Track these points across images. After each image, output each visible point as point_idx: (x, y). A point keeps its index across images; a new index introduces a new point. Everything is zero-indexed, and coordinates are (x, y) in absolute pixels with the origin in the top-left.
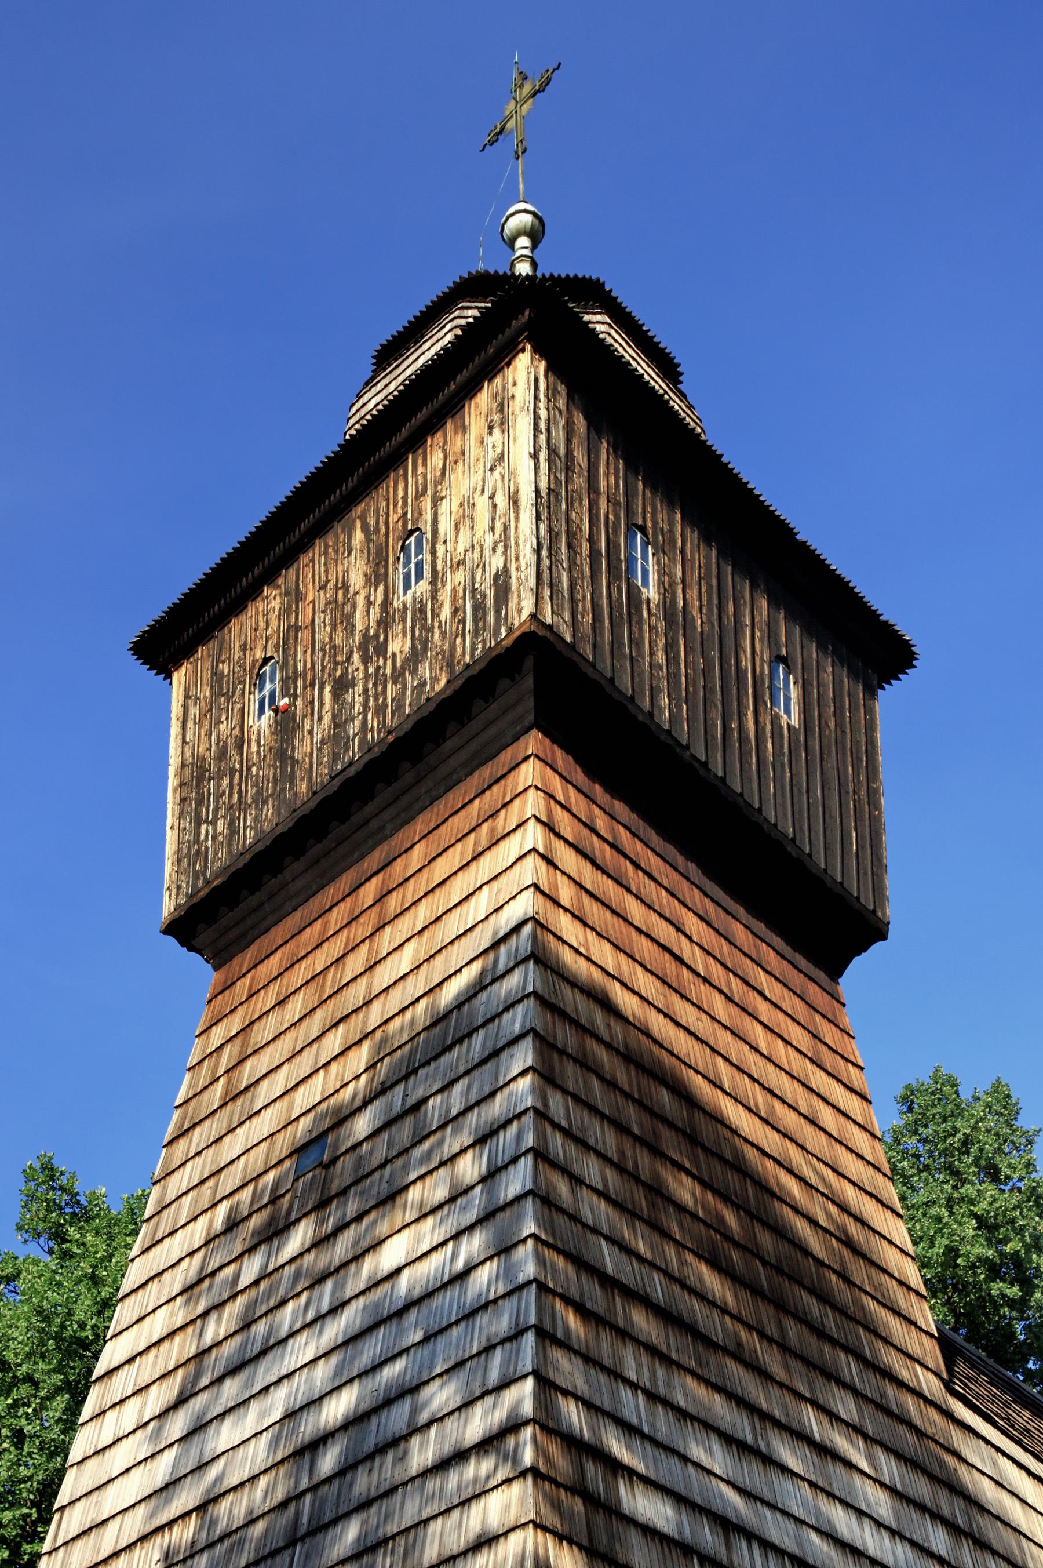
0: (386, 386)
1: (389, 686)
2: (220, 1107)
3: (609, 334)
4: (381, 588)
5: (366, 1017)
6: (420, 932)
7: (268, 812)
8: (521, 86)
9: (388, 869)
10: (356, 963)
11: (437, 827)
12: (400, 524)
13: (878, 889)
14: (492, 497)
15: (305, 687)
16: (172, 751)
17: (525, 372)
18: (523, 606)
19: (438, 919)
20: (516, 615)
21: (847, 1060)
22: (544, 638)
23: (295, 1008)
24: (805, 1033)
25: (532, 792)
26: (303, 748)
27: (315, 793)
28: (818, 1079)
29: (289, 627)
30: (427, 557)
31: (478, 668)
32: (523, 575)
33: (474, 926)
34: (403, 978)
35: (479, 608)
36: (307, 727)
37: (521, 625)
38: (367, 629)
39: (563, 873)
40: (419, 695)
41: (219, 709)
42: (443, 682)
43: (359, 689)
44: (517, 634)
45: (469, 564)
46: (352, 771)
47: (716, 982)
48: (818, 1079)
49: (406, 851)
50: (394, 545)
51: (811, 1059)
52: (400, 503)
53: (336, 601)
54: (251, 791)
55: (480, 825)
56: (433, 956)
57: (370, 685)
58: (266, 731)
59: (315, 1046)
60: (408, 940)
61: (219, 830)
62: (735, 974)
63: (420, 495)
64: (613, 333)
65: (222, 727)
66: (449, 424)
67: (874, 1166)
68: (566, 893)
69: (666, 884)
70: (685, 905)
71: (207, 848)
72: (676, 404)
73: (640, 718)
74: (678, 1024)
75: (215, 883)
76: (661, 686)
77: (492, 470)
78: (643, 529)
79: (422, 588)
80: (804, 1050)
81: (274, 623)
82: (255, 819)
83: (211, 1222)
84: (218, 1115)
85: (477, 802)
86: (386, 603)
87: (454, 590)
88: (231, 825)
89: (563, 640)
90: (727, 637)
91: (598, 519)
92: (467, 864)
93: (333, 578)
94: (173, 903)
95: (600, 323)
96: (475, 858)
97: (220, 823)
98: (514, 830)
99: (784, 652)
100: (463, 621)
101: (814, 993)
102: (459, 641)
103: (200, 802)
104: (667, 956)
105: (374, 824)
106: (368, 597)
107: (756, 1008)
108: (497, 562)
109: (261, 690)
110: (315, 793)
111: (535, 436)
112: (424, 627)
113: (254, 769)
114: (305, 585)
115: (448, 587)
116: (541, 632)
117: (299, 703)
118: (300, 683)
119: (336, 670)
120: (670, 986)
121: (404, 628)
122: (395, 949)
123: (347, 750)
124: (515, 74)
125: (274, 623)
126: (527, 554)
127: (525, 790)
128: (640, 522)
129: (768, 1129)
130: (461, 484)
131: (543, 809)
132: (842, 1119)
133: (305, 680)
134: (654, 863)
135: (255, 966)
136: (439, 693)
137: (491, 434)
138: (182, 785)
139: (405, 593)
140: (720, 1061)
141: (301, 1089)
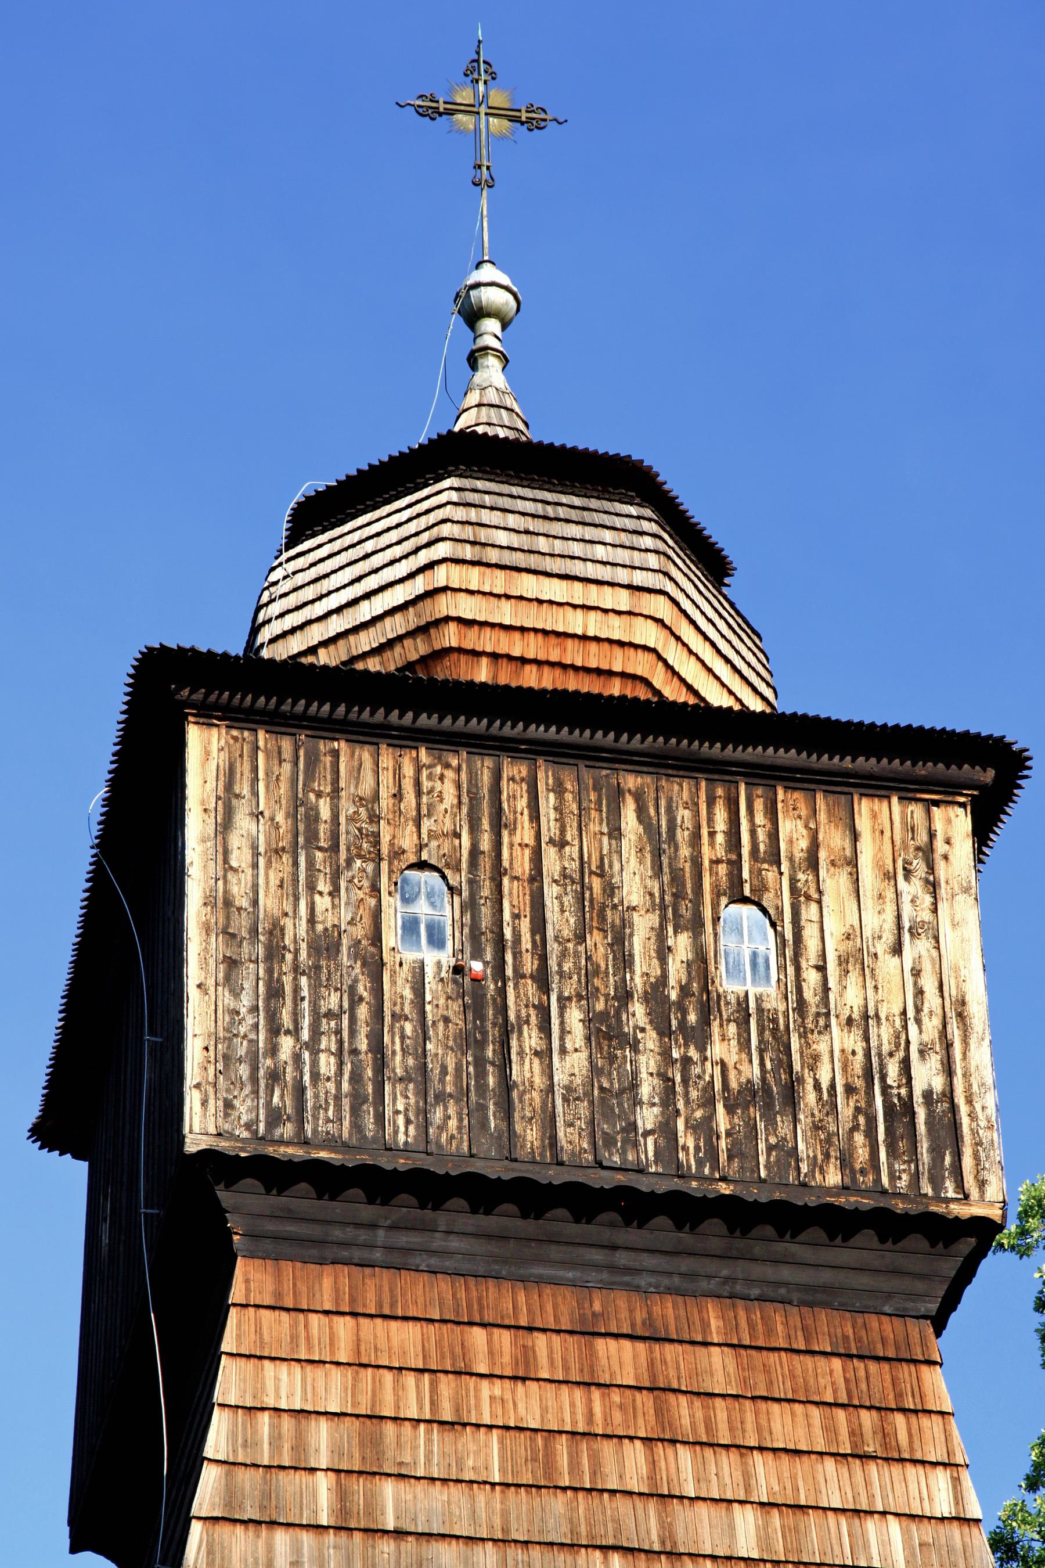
75: (323, 1155)
105: (622, 1258)
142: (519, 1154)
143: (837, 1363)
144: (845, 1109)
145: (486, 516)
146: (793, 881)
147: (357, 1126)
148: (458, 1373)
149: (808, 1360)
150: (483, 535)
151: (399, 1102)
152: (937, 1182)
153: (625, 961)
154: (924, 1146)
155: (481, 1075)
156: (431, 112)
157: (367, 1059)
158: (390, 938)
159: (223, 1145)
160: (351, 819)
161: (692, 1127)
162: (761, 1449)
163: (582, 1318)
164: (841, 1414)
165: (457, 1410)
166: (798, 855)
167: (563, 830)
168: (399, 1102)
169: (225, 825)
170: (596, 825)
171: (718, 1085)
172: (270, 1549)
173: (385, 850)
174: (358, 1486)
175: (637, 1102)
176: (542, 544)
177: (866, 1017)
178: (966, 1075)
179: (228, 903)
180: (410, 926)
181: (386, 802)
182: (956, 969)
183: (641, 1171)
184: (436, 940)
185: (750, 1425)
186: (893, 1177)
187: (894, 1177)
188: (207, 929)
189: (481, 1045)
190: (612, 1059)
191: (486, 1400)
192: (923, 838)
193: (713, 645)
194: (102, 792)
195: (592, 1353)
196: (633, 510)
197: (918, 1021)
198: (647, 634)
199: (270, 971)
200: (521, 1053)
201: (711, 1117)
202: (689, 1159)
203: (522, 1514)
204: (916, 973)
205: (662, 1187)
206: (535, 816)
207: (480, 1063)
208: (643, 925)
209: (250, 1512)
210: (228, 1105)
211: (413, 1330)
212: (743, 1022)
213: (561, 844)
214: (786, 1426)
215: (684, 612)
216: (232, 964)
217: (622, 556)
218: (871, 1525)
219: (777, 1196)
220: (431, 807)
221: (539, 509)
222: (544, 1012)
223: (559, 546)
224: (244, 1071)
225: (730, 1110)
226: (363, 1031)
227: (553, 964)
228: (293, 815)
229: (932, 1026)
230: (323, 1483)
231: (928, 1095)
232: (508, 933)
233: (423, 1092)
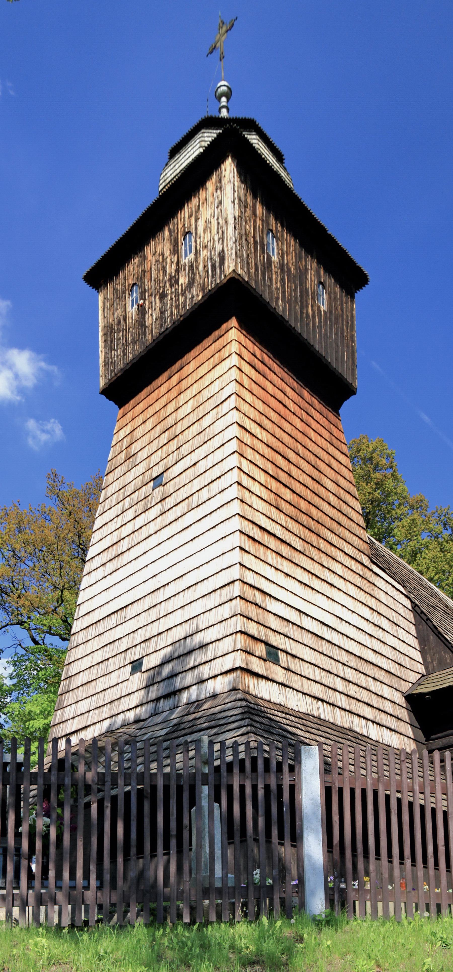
0: (174, 166)
1: (180, 297)
2: (124, 462)
3: (258, 144)
4: (176, 256)
5: (175, 429)
6: (194, 396)
7: (137, 347)
8: (222, 27)
9: (181, 371)
10: (171, 408)
11: (199, 355)
12: (182, 229)
13: (353, 374)
14: (218, 219)
15: (148, 296)
16: (100, 321)
17: (229, 168)
18: (230, 266)
19: (200, 391)
20: (227, 270)
21: (341, 442)
22: (238, 280)
23: (149, 424)
24: (327, 432)
25: (234, 342)
26: (149, 321)
27: (154, 340)
28: (331, 450)
29: (142, 271)
30: (193, 244)
31: (213, 291)
32: (230, 253)
33: (214, 395)
34: (188, 414)
35: (213, 266)
36: (150, 313)
37: (230, 274)
38: (171, 273)
39: (245, 374)
40: (192, 301)
41: (117, 304)
42: (200, 297)
43: (169, 297)
44: (228, 278)
45: (209, 248)
46: (167, 332)
47: (297, 414)
48: (331, 450)
49: (188, 364)
50: (180, 238)
51: (329, 442)
52: (182, 220)
53: (159, 261)
54: (130, 338)
55: (215, 354)
56: (199, 406)
57: (173, 297)
58: (135, 314)
59: (158, 439)
60: (190, 399)
61: (119, 353)
62: (304, 411)
63: (190, 217)
64: (260, 143)
65: (118, 311)
66: (201, 190)
67: (350, 482)
68: (246, 382)
69: (280, 376)
70: (287, 384)
71: (115, 361)
72: (283, 174)
73: (272, 310)
74: (284, 431)
75: (119, 375)
76: (277, 295)
77: (217, 207)
78: (272, 231)
79: (192, 256)
80: (327, 439)
81: (136, 269)
82: (132, 349)
83: (124, 505)
84: (123, 464)
85: (213, 345)
86: (178, 262)
87: (204, 258)
88: (123, 351)
89: (244, 280)
90: (302, 275)
91: (256, 228)
92: (211, 370)
93: (158, 250)
94: (104, 382)
95: (254, 139)
96: (213, 368)
97: (119, 351)
98: (227, 357)
99: (322, 280)
100: (207, 271)
101: (331, 416)
102: (206, 279)
103: (111, 342)
104: (281, 405)
106: (171, 260)
107: (311, 423)
108: (219, 248)
109: (132, 297)
110: (154, 340)
111: (234, 194)
112: (193, 273)
113: (131, 329)
114: (147, 254)
115: (202, 257)
116: (237, 277)
117: (147, 302)
118: (147, 294)
119: (160, 289)
120: (282, 417)
121: (185, 273)
122: (185, 403)
123: (165, 323)
124: (220, 21)
125: (136, 269)
126: (231, 243)
127: (231, 341)
128: (271, 228)
129: (315, 470)
130: (205, 213)
131: (238, 349)
132: (339, 464)
133: (148, 293)
134: (276, 368)
135: (134, 408)
136: (199, 301)
137: (217, 192)
138: (105, 334)
139: (185, 258)
140: (299, 444)
141: (153, 455)
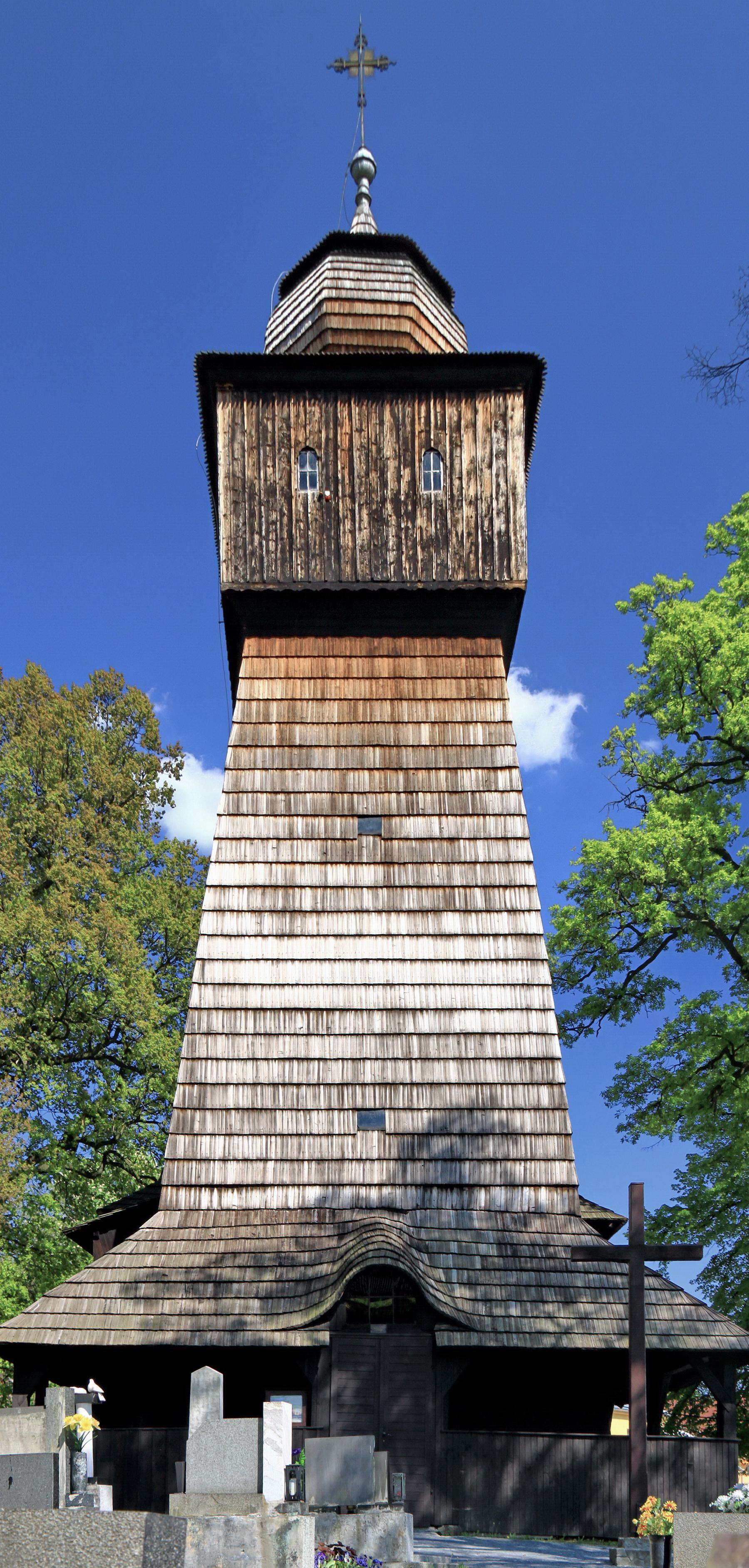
75: (271, 587)
142: (343, 579)
143: (463, 660)
144: (467, 544)
145: (342, 274)
146: (451, 437)
147: (283, 573)
148: (323, 678)
149: (452, 659)
150: (340, 283)
151: (298, 559)
152: (501, 574)
153: (384, 484)
154: (496, 558)
155: (329, 544)
156: (341, 69)
157: (286, 541)
158: (295, 485)
159: (235, 586)
160: (280, 429)
161: (408, 559)
162: (433, 699)
163: (370, 650)
164: (463, 681)
165: (323, 693)
166: (453, 425)
167: (361, 425)
168: (298, 559)
169: (232, 440)
170: (374, 420)
171: (418, 539)
172: (255, 755)
173: (293, 443)
174: (286, 728)
175: (388, 550)
176: (364, 285)
177: (477, 499)
178: (515, 522)
179: (234, 475)
180: (303, 476)
181: (292, 420)
182: (513, 472)
183: (388, 581)
184: (313, 485)
185: (430, 691)
186: (484, 573)
187: (483, 573)
188: (226, 488)
189: (329, 530)
190: (378, 531)
191: (333, 688)
192: (502, 409)
193: (437, 329)
194: (201, 436)
195: (373, 665)
196: (401, 262)
197: (497, 499)
198: (407, 327)
199: (250, 505)
200: (344, 532)
201: (415, 553)
202: (406, 574)
203: (346, 734)
204: (497, 476)
205: (397, 587)
206: (350, 419)
207: (329, 538)
208: (392, 464)
209: (249, 742)
210: (236, 568)
211: (308, 661)
212: (429, 509)
213: (360, 431)
214: (445, 689)
215: (422, 313)
216: (235, 503)
217: (396, 286)
218: (471, 727)
219: (440, 586)
220: (310, 419)
221: (363, 267)
222: (353, 511)
223: (371, 285)
224: (241, 552)
225: (423, 549)
226: (285, 529)
227: (357, 490)
228: (257, 431)
229: (502, 499)
230: (274, 727)
231: (499, 533)
232: (340, 476)
233: (307, 555)
